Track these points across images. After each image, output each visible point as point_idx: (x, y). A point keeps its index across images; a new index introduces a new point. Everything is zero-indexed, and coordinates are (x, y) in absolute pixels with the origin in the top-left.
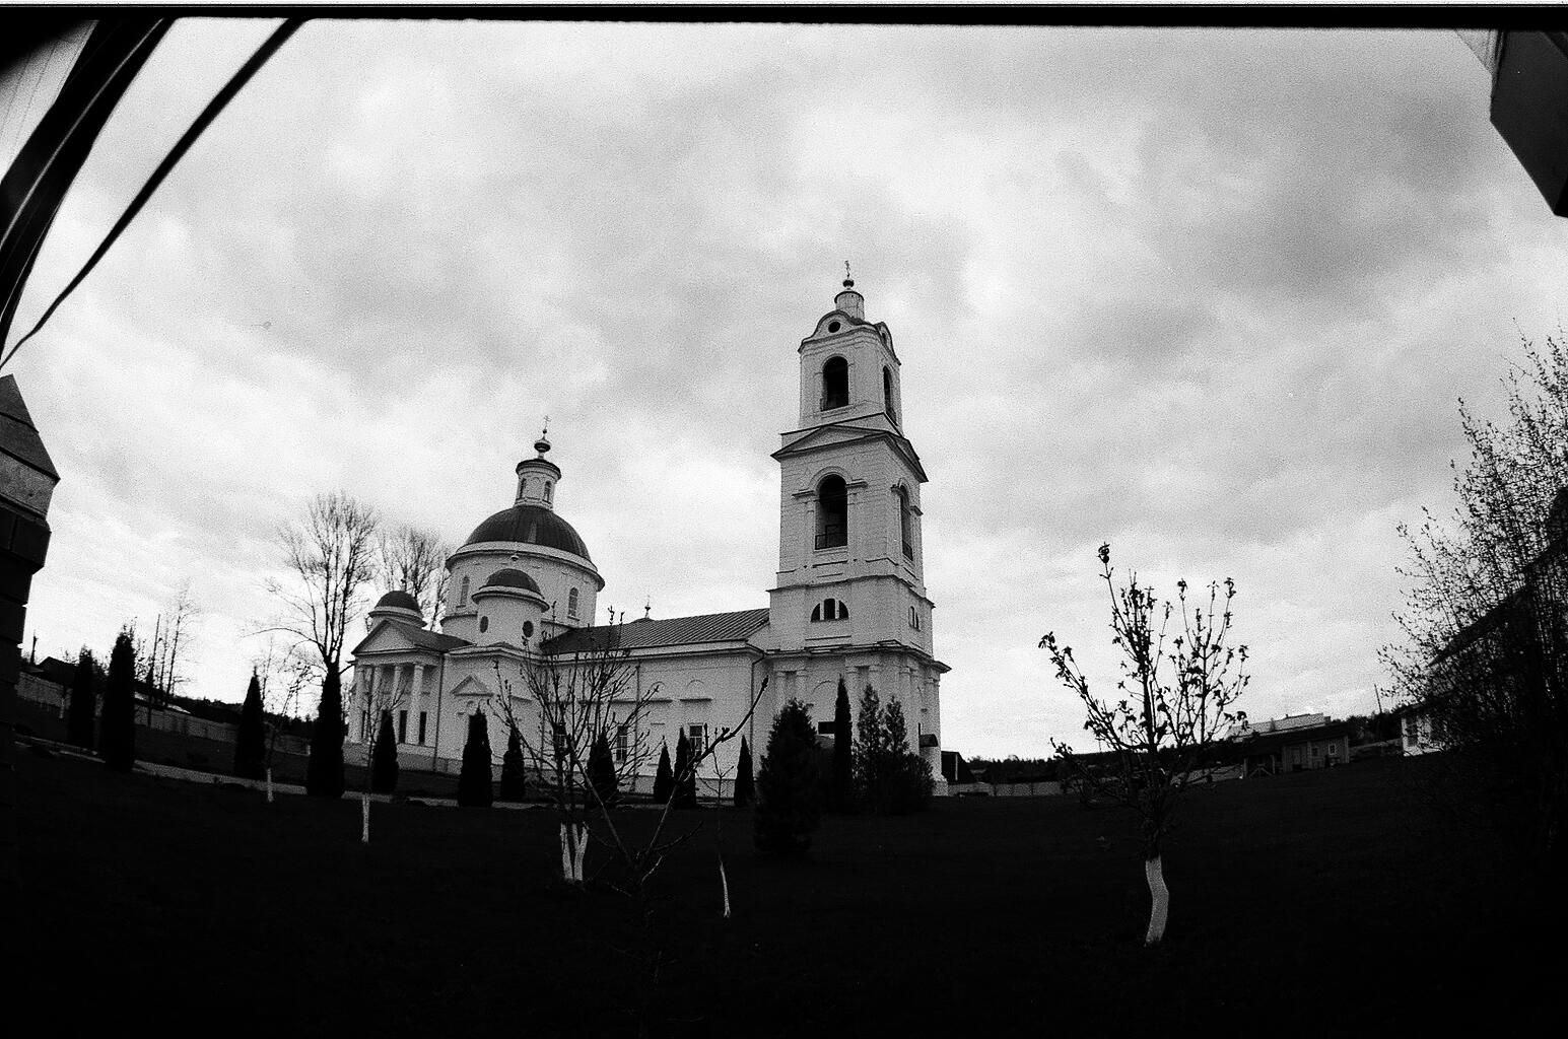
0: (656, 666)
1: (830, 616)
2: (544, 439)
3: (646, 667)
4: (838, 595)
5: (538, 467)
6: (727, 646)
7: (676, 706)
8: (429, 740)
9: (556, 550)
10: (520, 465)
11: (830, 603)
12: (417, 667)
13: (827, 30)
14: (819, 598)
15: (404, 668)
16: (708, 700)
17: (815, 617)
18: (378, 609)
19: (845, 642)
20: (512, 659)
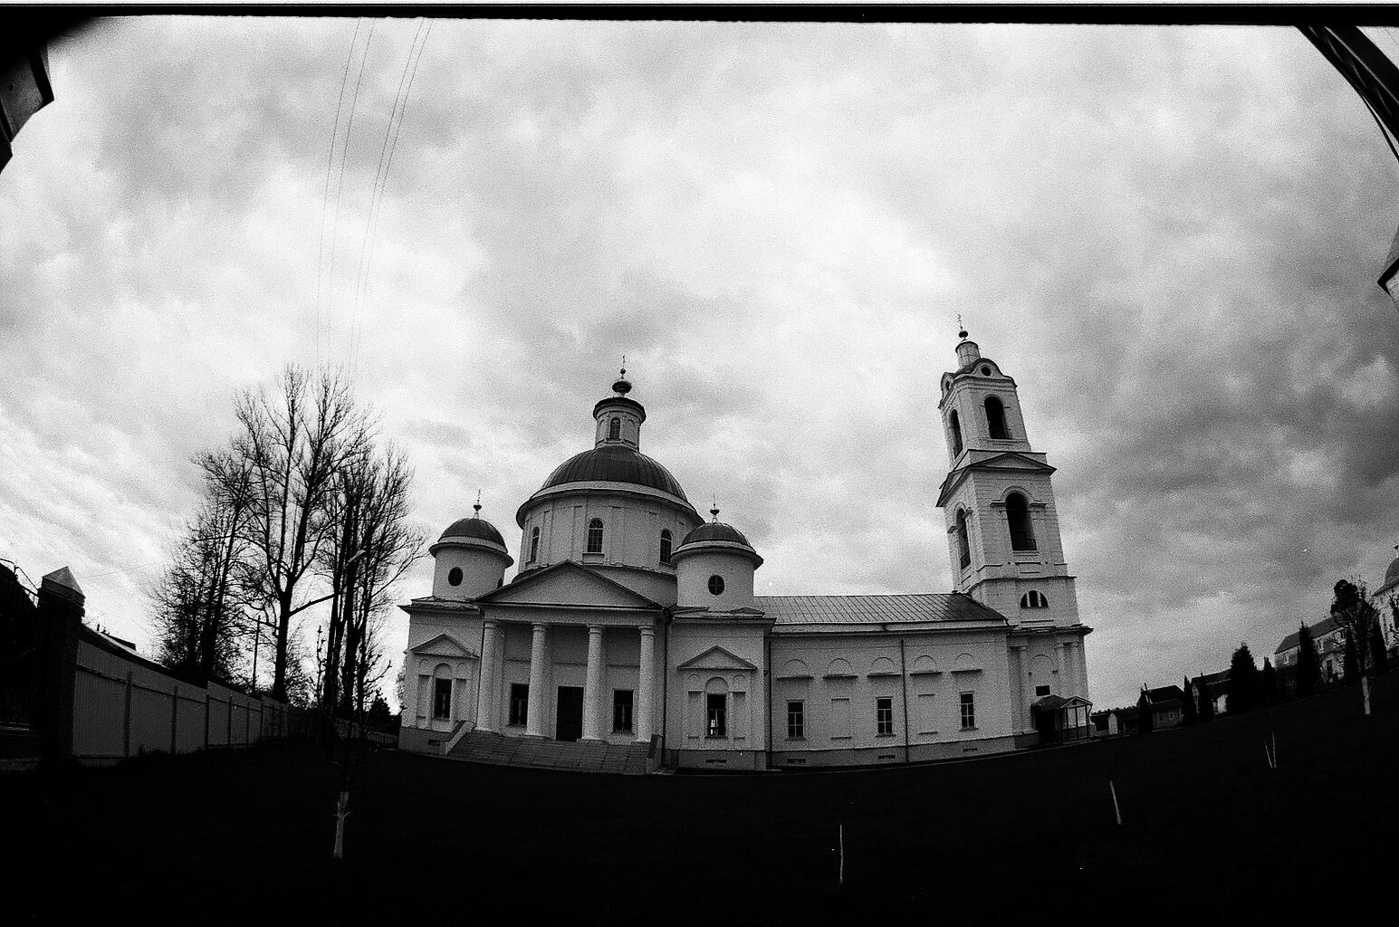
0: (919, 642)
1: (1034, 604)
2: (622, 378)
3: (908, 642)
4: (1039, 589)
5: (621, 407)
6: (989, 624)
7: (862, 674)
8: (898, 726)
9: (633, 485)
10: (601, 403)
11: (1033, 594)
12: (644, 632)
13: (524, 22)
14: (1026, 590)
15: (547, 629)
16: (979, 671)
17: (1023, 604)
18: (446, 540)
19: (1051, 624)
20: (737, 624)
